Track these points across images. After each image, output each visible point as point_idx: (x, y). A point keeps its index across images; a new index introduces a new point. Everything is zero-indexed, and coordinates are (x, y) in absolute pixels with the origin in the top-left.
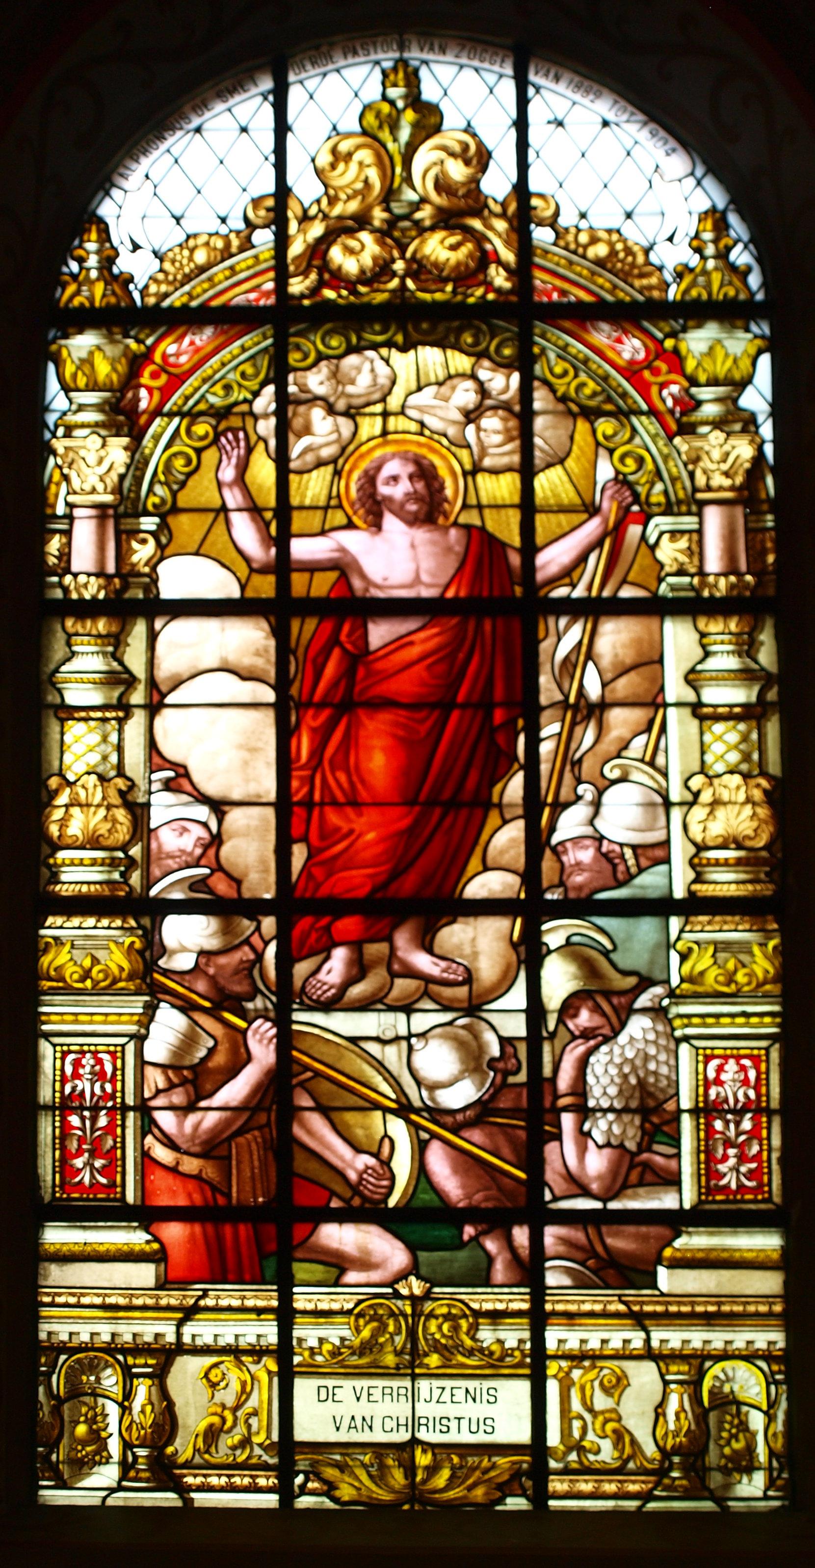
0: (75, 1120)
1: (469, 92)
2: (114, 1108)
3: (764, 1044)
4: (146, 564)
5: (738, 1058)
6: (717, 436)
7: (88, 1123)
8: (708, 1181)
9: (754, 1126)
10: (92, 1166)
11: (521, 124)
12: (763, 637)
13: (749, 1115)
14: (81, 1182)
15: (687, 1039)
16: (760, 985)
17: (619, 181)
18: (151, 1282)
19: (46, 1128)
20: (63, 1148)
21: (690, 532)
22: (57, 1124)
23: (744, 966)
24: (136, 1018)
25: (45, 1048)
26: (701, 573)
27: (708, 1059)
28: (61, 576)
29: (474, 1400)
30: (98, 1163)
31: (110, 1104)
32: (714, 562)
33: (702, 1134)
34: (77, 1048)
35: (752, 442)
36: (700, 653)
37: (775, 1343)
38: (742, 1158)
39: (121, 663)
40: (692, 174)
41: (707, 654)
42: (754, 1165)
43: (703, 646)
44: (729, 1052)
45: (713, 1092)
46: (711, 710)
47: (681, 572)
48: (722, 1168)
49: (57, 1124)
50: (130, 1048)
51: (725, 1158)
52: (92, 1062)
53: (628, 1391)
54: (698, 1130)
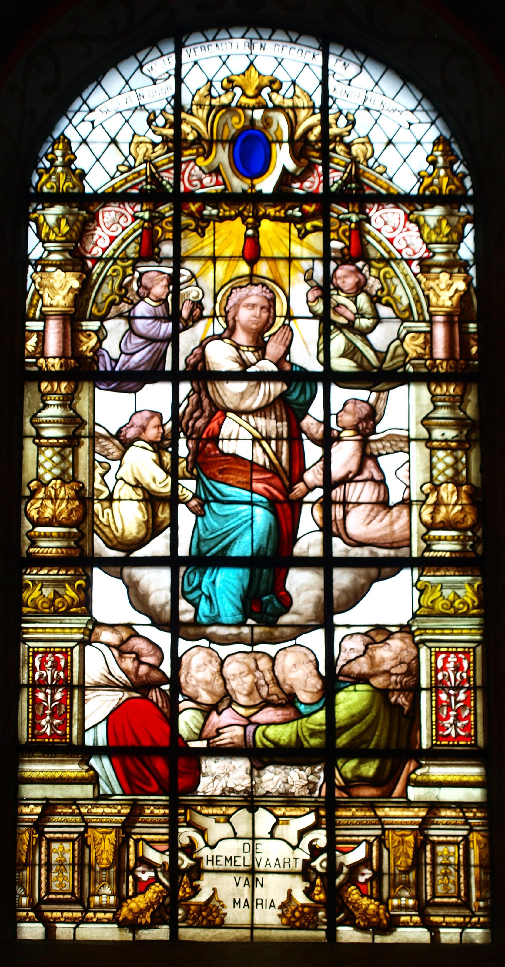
0: (443, 697)
2: (469, 689)
4: (91, 351)
5: (456, 653)
6: (444, 277)
7: (49, 697)
8: (33, 731)
9: (466, 698)
10: (52, 724)
12: (470, 397)
13: (463, 691)
14: (449, 735)
15: (423, 642)
16: (69, 608)
17: (393, 128)
20: (437, 714)
21: (424, 332)
22: (434, 698)
23: (60, 596)
24: (82, 631)
26: (432, 358)
27: (438, 654)
28: (38, 359)
30: (56, 722)
31: (467, 685)
32: (440, 351)
33: (434, 703)
34: (445, 649)
35: (465, 280)
36: (432, 407)
38: (458, 718)
39: (75, 411)
41: (436, 408)
42: (467, 722)
43: (433, 402)
44: (450, 650)
45: (440, 676)
46: (45, 441)
48: (446, 724)
49: (434, 698)
50: (76, 650)
51: (448, 717)
52: (455, 660)
54: (432, 700)
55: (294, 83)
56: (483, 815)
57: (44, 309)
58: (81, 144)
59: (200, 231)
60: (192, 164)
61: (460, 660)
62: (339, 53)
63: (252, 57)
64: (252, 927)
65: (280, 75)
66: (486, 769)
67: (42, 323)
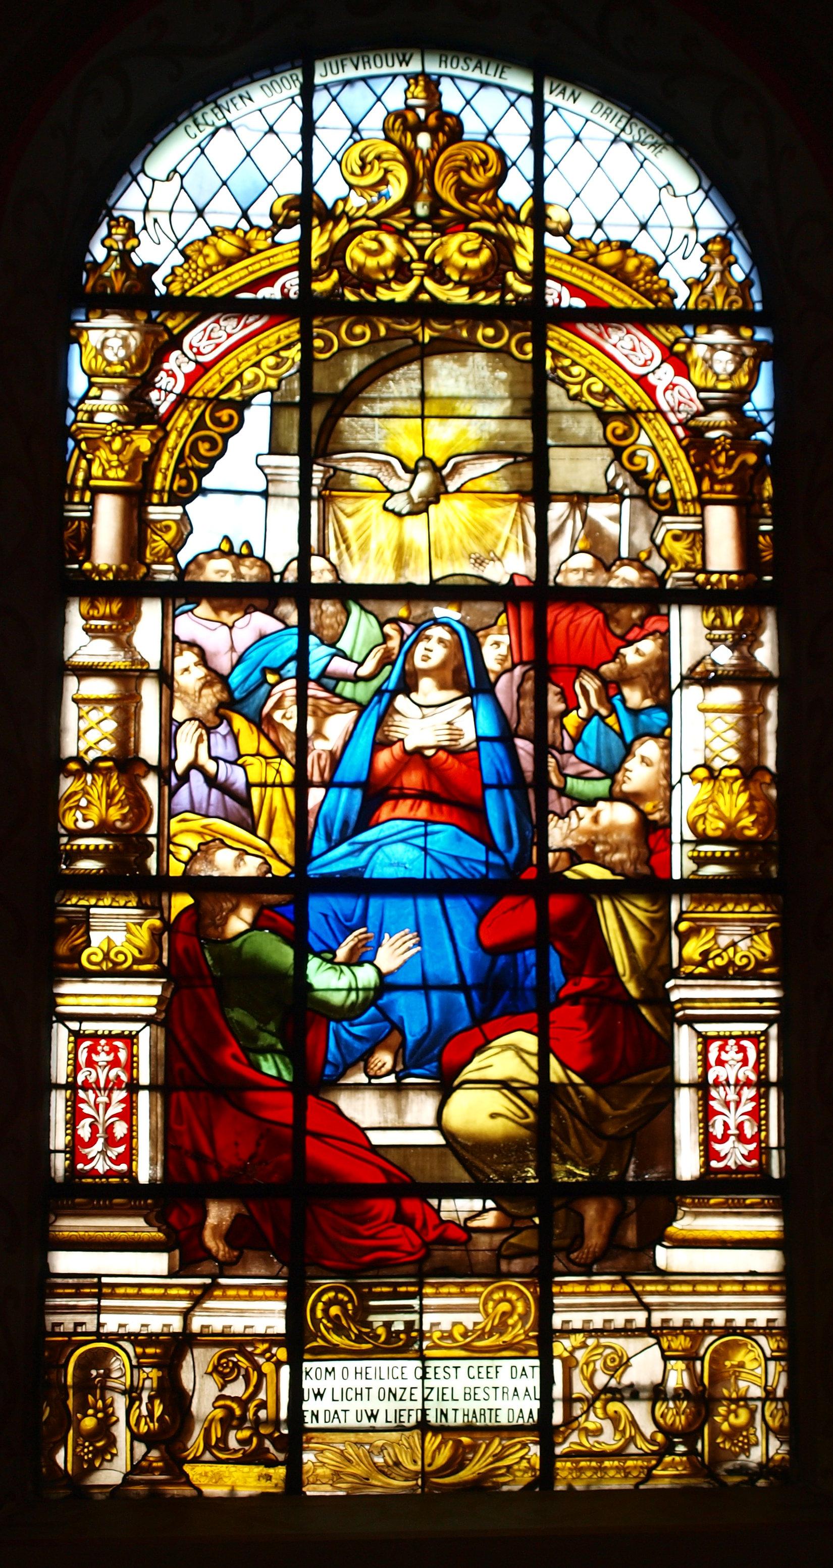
1: (488, 104)
3: (762, 1027)
11: (537, 140)
18: (164, 1269)
19: (58, 1102)
25: (61, 1037)
29: (390, 1390)
30: (114, 1152)
37: (774, 1320)
40: (700, 187)
47: (686, 569)
53: (629, 1370)
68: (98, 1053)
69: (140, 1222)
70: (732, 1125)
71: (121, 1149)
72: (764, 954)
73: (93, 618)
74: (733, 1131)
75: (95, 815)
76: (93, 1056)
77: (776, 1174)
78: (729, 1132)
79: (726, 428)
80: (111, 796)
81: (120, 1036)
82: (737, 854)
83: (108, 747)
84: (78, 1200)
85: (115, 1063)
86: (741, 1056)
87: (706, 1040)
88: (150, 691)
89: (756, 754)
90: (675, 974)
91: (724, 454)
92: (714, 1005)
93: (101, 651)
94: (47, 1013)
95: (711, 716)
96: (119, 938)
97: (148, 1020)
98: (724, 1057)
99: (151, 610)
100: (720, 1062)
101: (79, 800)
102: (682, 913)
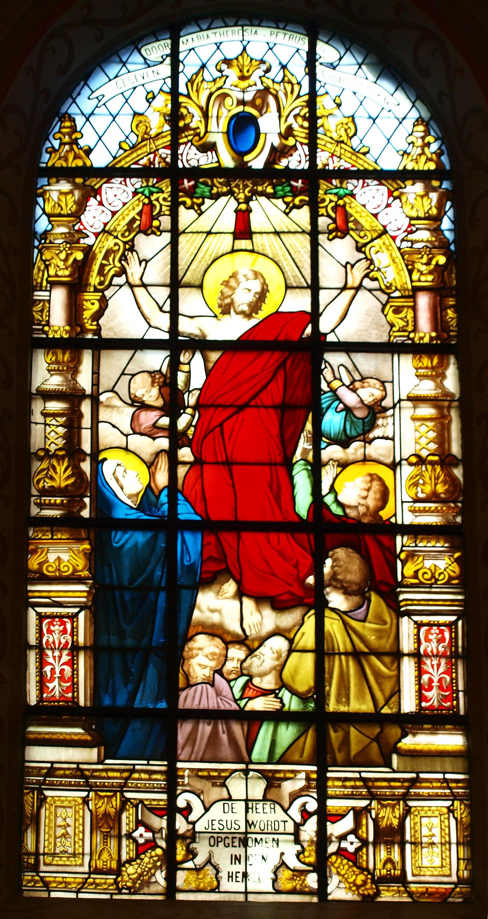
3: (453, 618)
17: (374, 115)
25: (32, 615)
52: (437, 631)
55: (284, 67)
56: (465, 785)
57: (50, 279)
58: (92, 114)
59: (196, 208)
60: (190, 144)
61: (442, 632)
62: (326, 40)
63: (245, 43)
64: (246, 893)
65: (270, 59)
66: (445, 180)
67: (48, 293)
68: (54, 626)
69: (80, 731)
70: (436, 679)
71: (68, 684)
72: (454, 572)
73: (421, 368)
74: (435, 684)
75: (428, 489)
76: (51, 627)
77: (462, 712)
78: (55, 676)
79: (428, 241)
80: (437, 478)
81: (67, 616)
82: (65, 501)
83: (433, 446)
84: (64, 717)
85: (64, 631)
86: (62, 628)
87: (419, 625)
88: (86, 407)
89: (446, 446)
90: (401, 585)
91: (64, 252)
92: (431, 603)
93: (55, 382)
94: (25, 603)
95: (418, 423)
96: (65, 557)
97: (82, 607)
98: (52, 628)
99: (87, 358)
100: (50, 632)
101: (418, 480)
102: (403, 546)
